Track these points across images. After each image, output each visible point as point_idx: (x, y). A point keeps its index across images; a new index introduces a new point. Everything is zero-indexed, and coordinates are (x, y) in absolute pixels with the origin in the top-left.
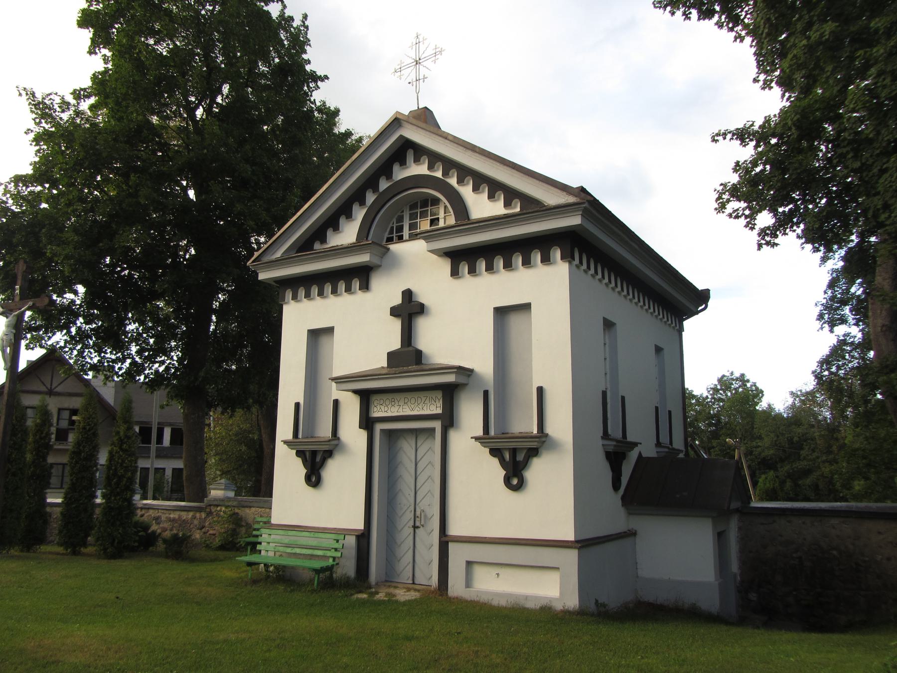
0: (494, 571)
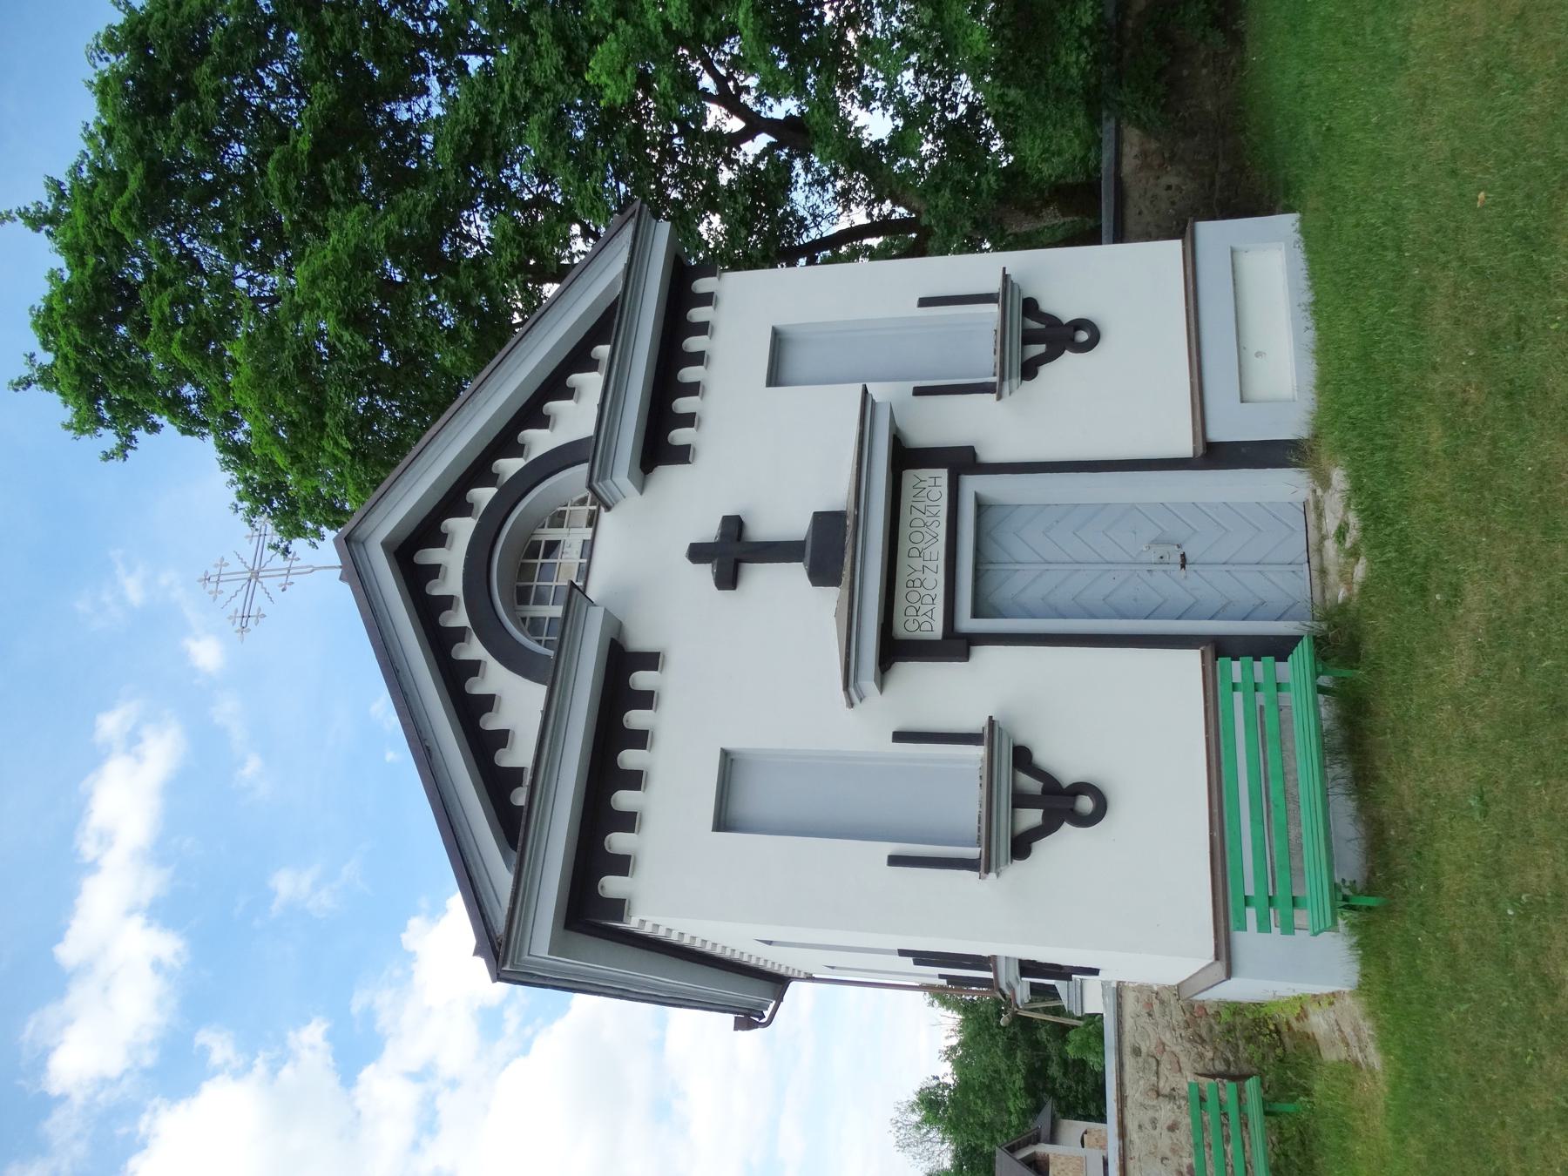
0: (1254, 364)
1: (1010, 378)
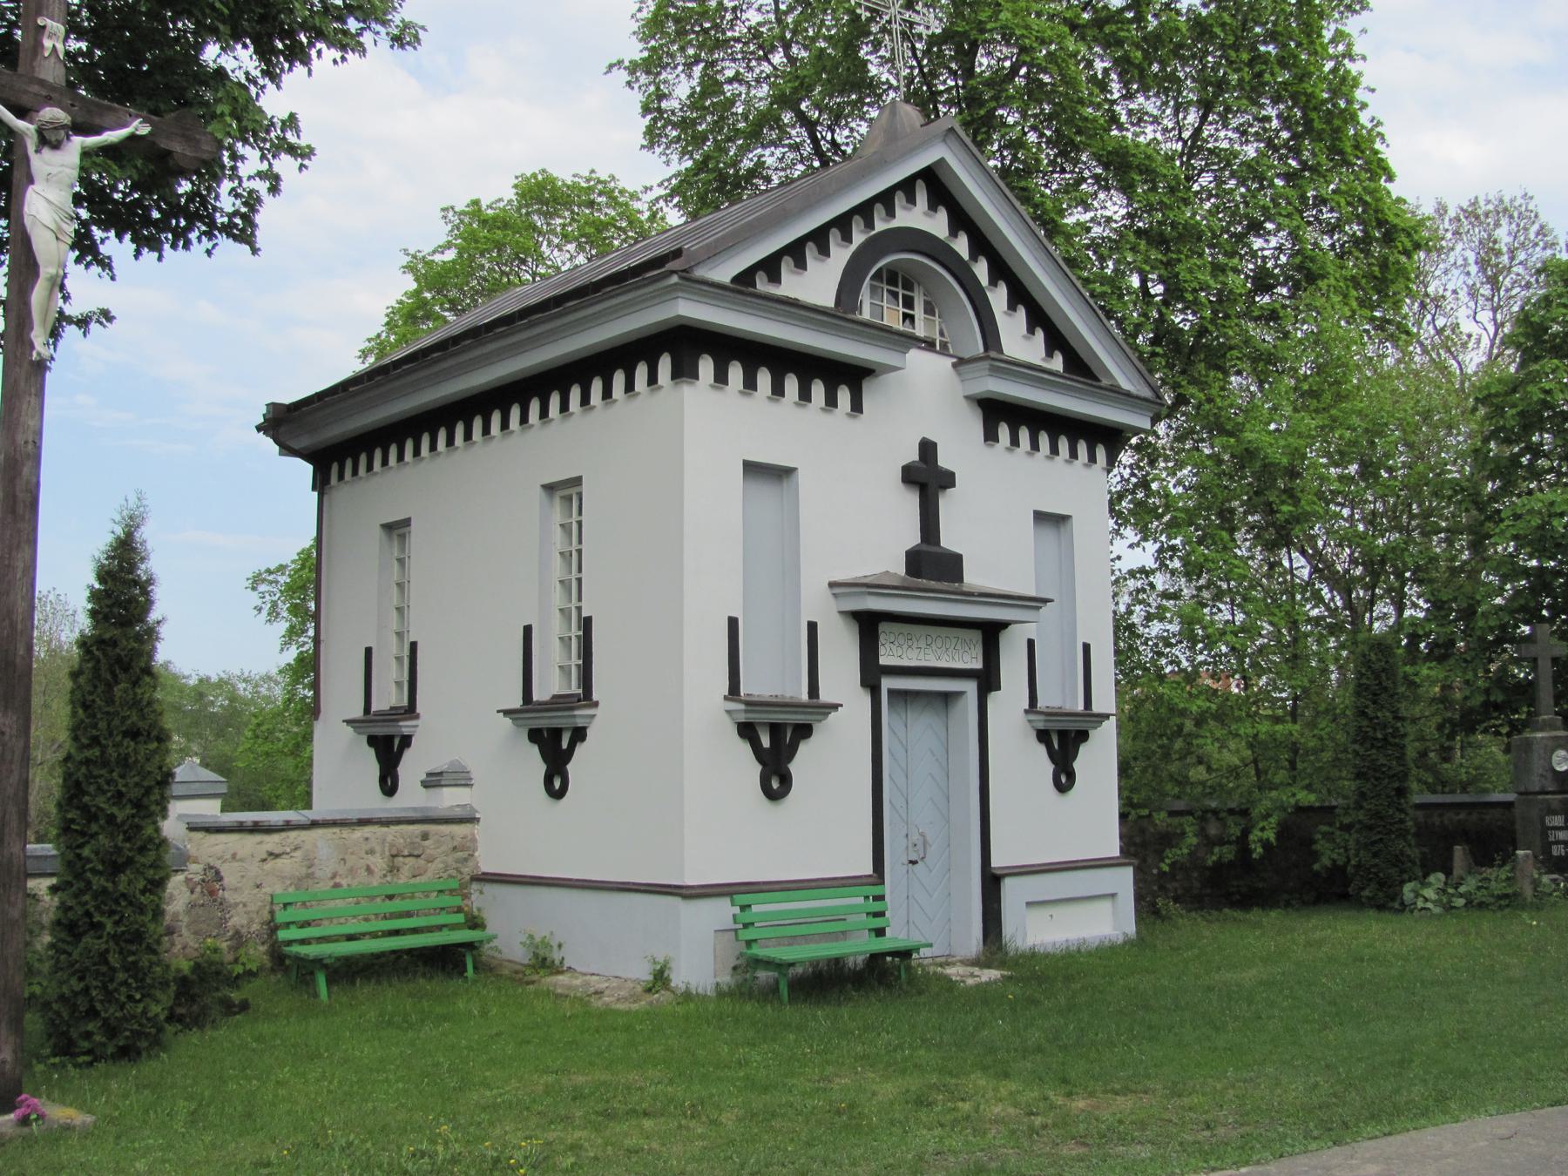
1: (1046, 721)
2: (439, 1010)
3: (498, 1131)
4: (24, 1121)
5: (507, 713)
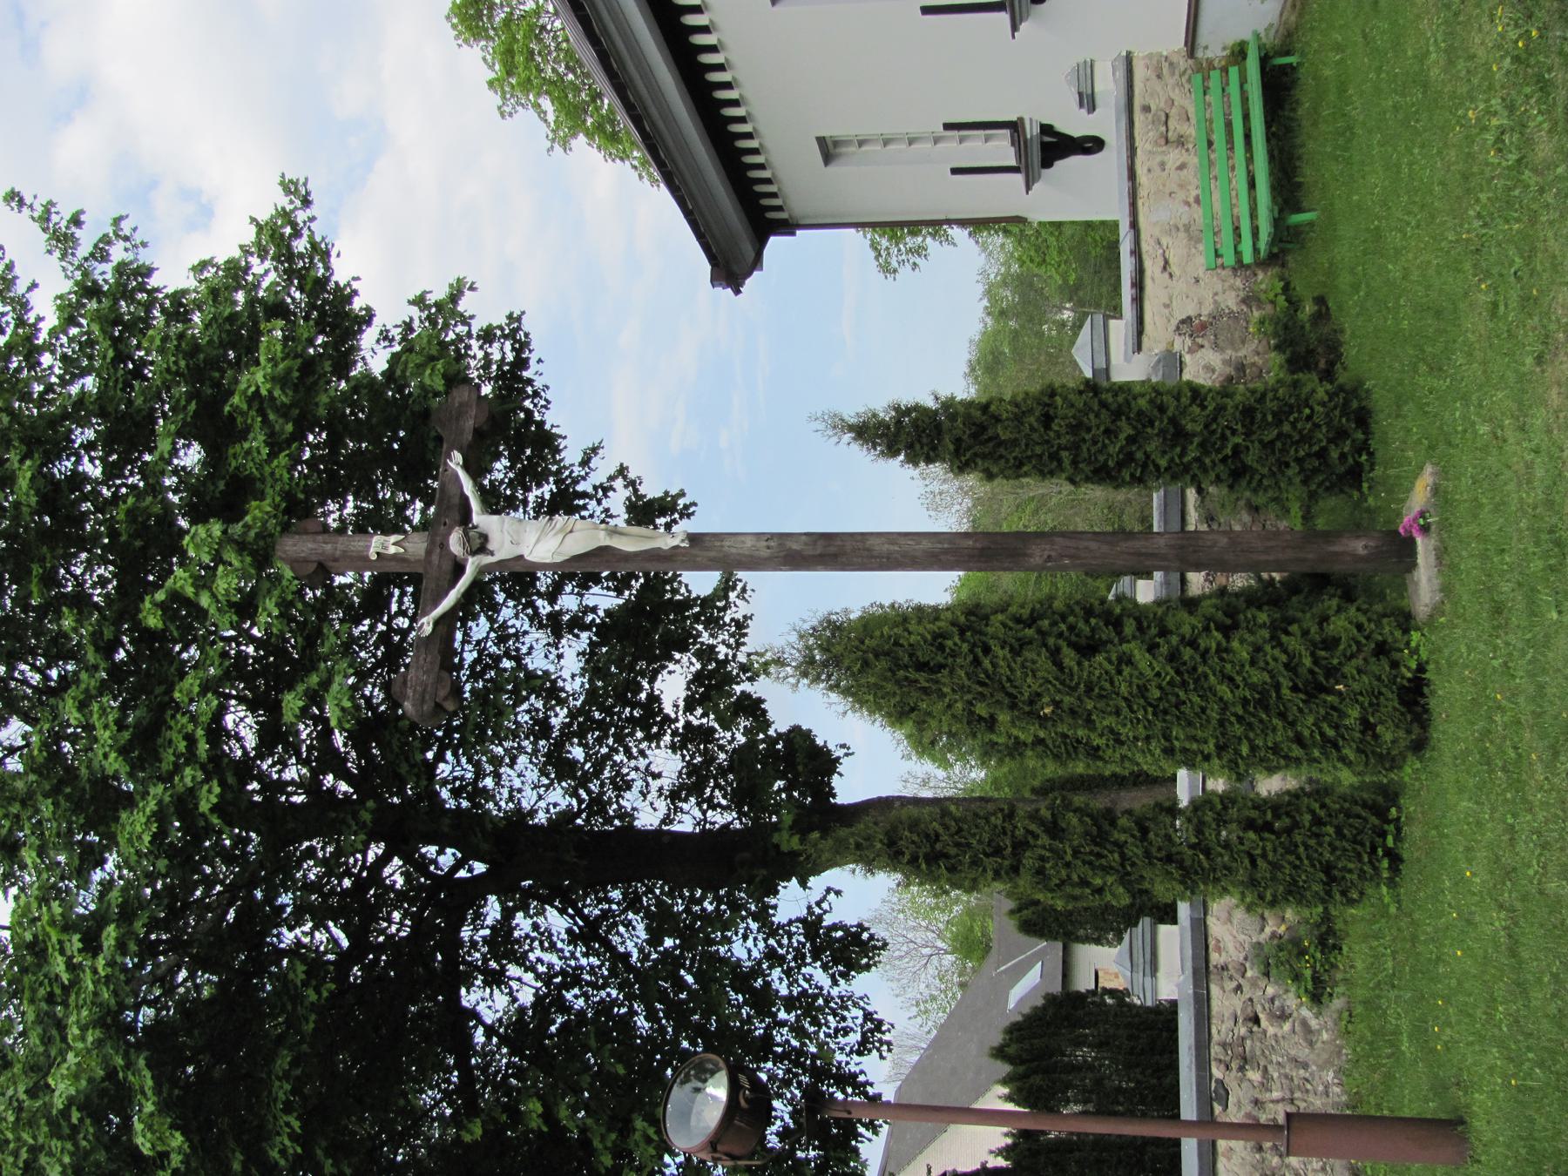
2: (1332, 97)
3: (1481, 53)
4: (1425, 529)
5: (1015, 28)
